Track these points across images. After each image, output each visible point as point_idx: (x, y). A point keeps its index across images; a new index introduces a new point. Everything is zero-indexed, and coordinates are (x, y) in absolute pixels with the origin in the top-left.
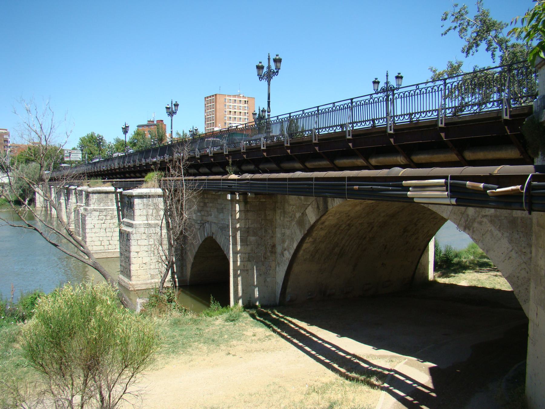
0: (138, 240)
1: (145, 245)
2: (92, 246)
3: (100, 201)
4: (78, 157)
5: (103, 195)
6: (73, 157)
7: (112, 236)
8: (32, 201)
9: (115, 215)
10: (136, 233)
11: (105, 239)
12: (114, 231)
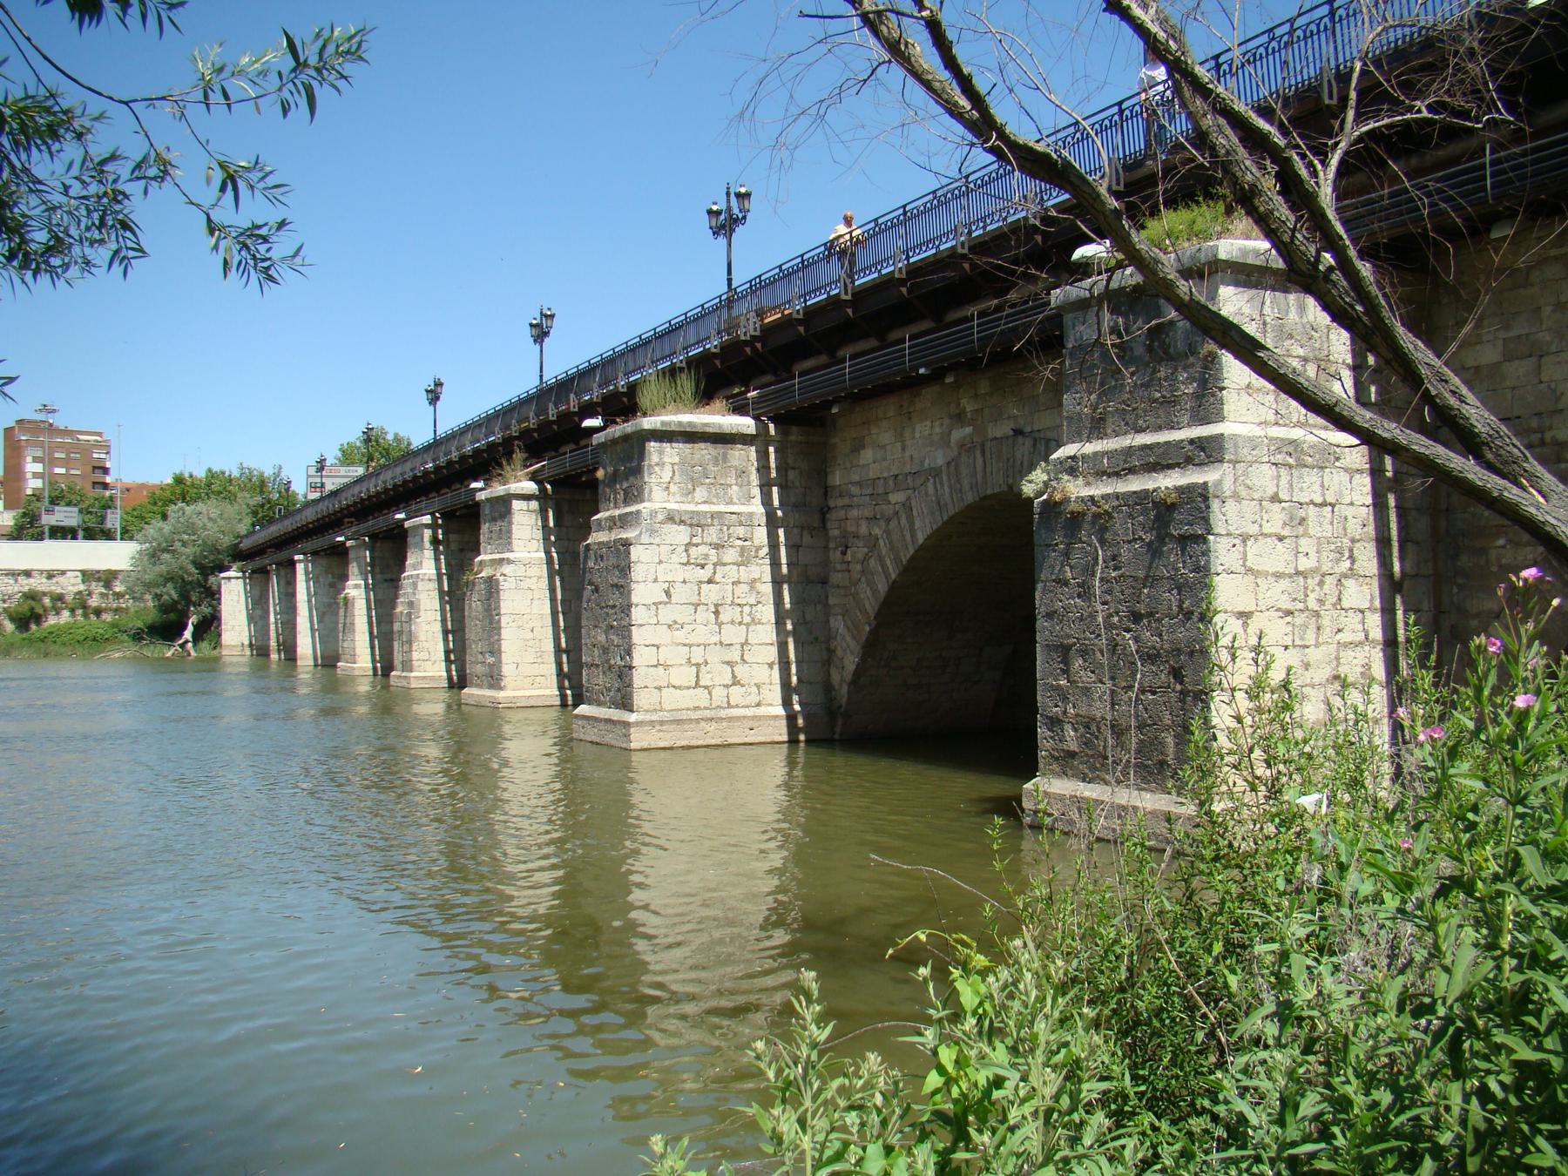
0: (1245, 538)
1: (1278, 576)
2: (659, 688)
3: (692, 479)
5: (704, 451)
7: (747, 642)
8: (209, 626)
9: (757, 542)
10: (1236, 496)
11: (715, 656)
12: (755, 621)
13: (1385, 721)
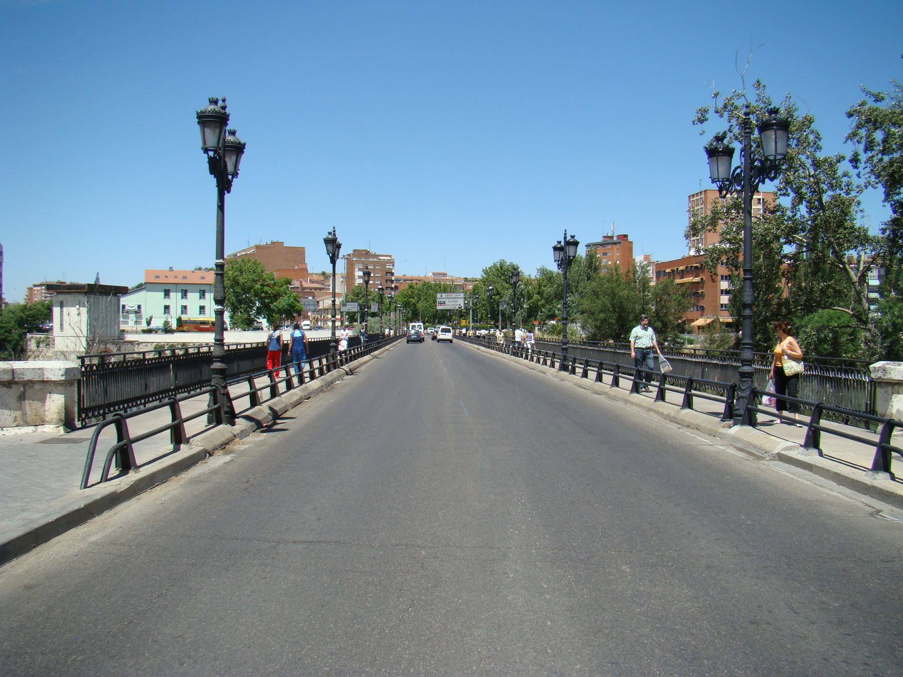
4: (457, 303)
6: (450, 303)
13: (762, 210)
